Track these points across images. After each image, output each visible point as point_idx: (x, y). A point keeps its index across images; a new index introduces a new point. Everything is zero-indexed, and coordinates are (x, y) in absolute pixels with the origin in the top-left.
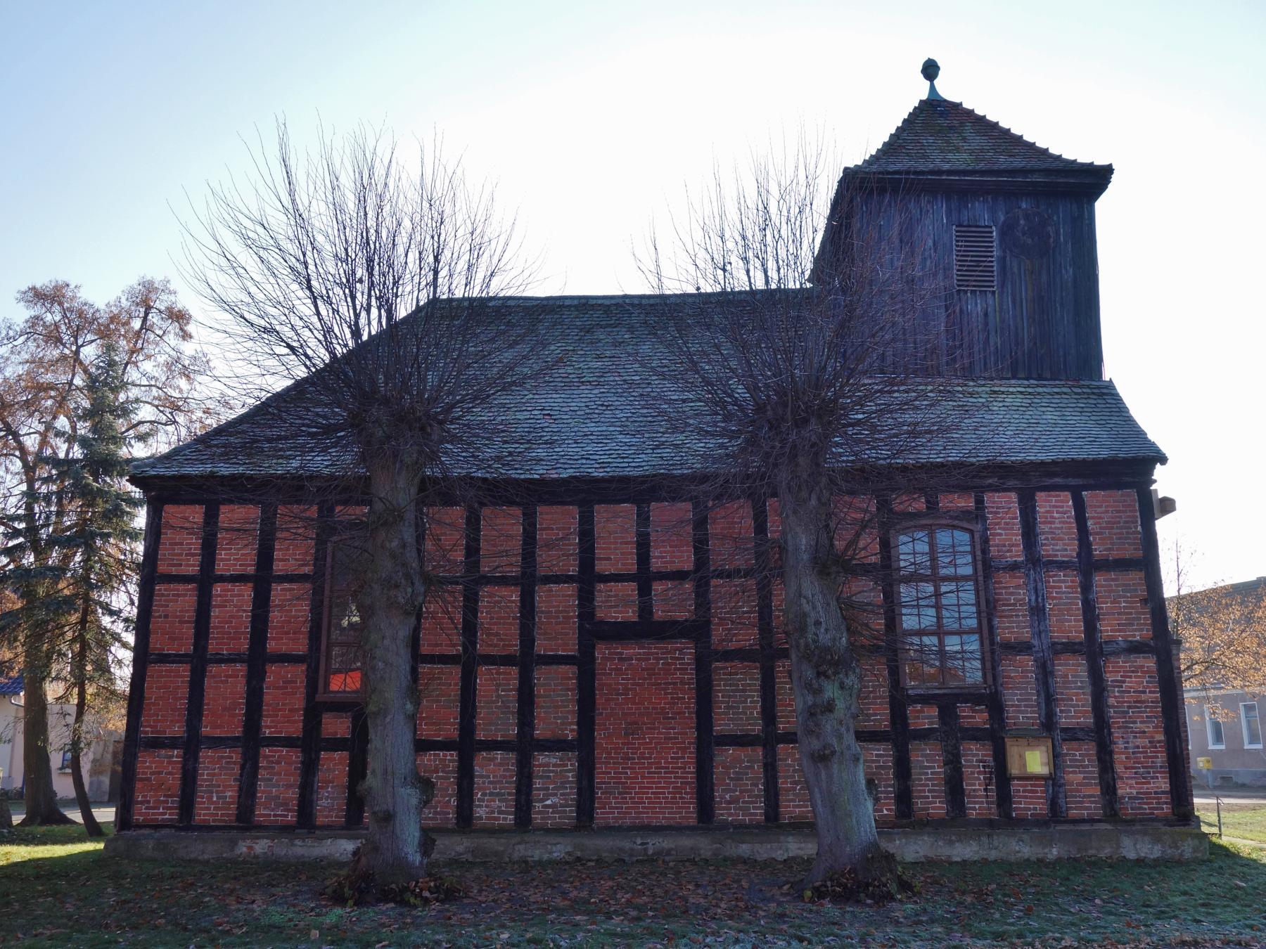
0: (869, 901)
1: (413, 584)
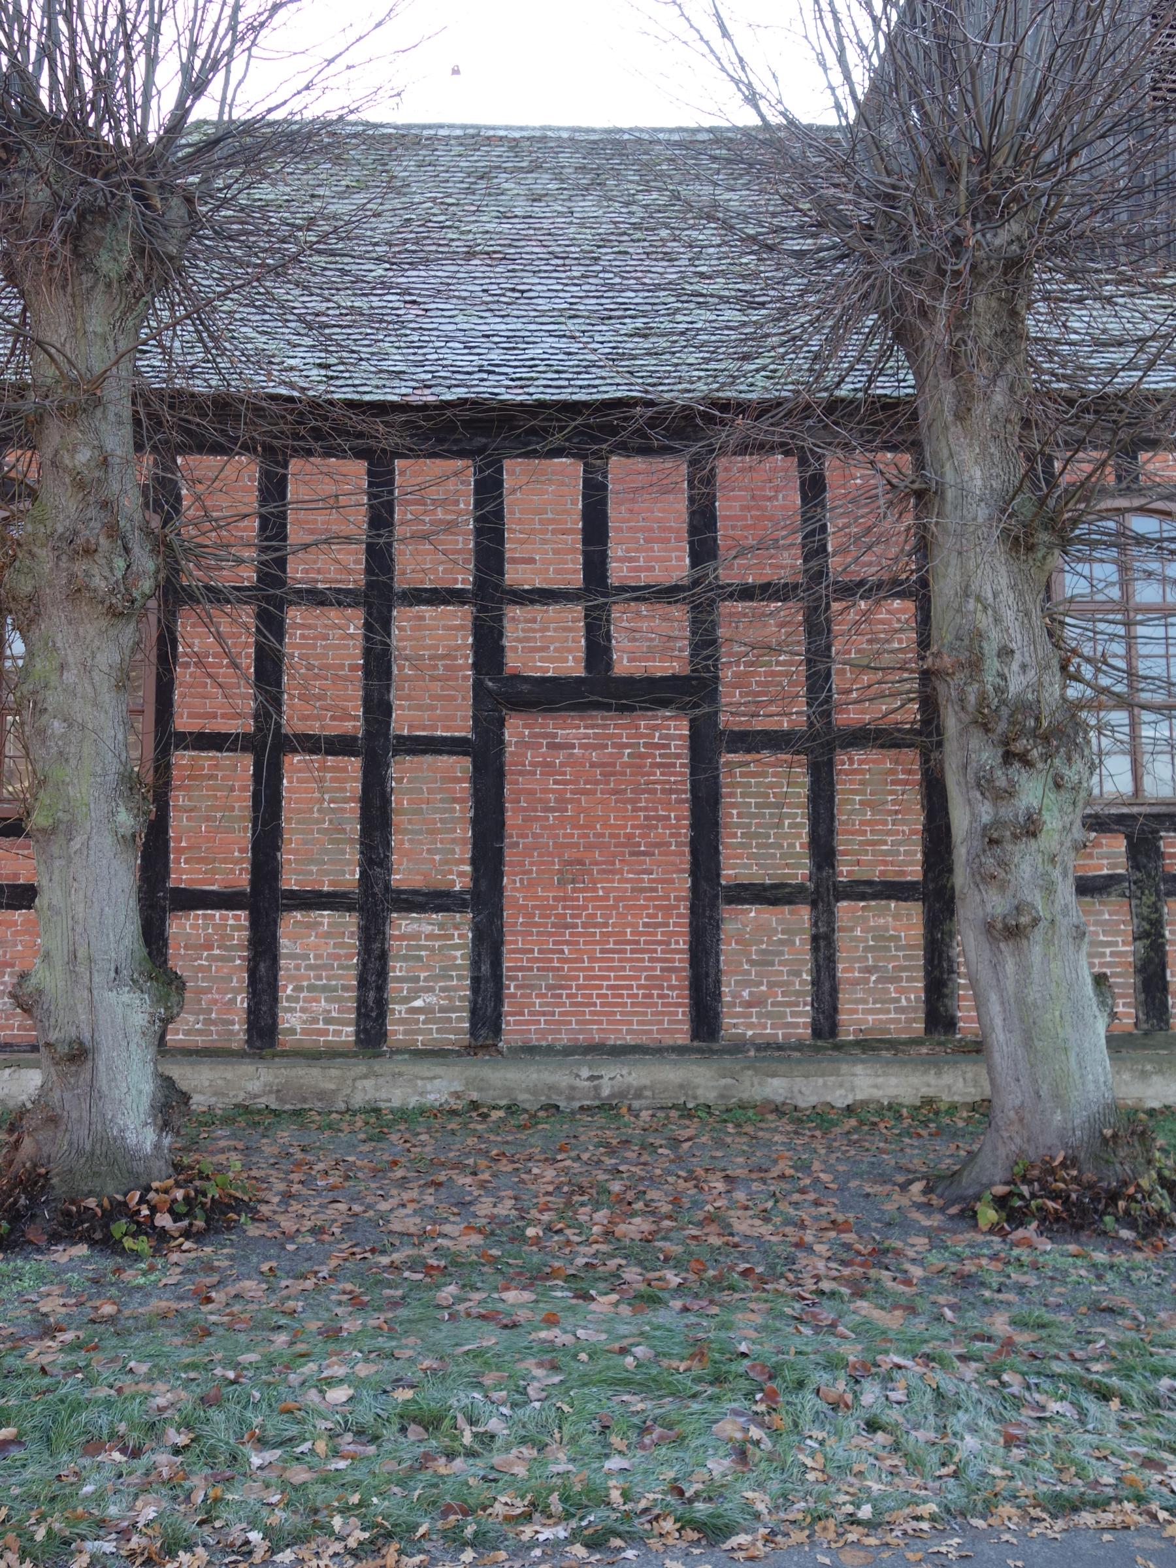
0: (1125, 1234)
1: (127, 550)
